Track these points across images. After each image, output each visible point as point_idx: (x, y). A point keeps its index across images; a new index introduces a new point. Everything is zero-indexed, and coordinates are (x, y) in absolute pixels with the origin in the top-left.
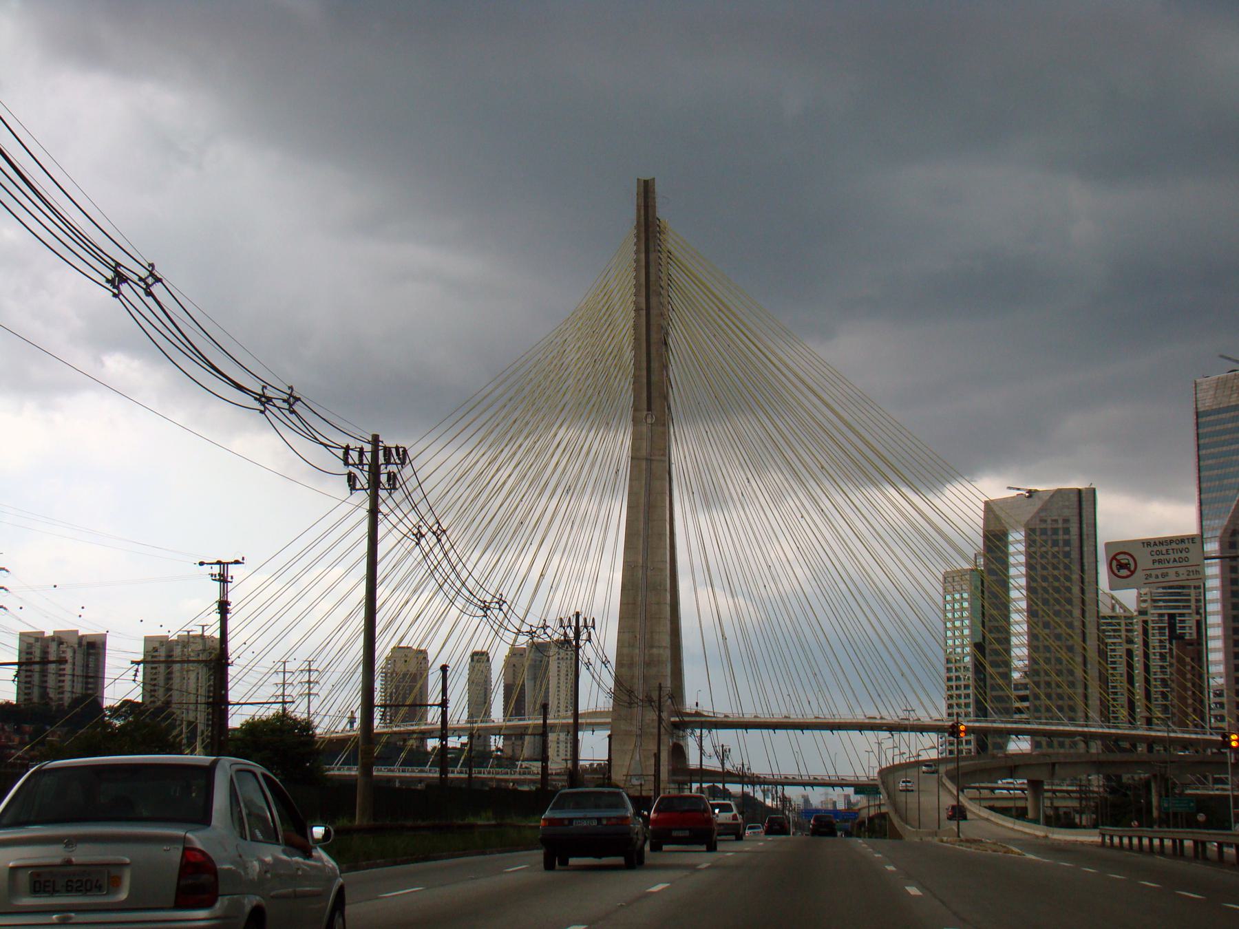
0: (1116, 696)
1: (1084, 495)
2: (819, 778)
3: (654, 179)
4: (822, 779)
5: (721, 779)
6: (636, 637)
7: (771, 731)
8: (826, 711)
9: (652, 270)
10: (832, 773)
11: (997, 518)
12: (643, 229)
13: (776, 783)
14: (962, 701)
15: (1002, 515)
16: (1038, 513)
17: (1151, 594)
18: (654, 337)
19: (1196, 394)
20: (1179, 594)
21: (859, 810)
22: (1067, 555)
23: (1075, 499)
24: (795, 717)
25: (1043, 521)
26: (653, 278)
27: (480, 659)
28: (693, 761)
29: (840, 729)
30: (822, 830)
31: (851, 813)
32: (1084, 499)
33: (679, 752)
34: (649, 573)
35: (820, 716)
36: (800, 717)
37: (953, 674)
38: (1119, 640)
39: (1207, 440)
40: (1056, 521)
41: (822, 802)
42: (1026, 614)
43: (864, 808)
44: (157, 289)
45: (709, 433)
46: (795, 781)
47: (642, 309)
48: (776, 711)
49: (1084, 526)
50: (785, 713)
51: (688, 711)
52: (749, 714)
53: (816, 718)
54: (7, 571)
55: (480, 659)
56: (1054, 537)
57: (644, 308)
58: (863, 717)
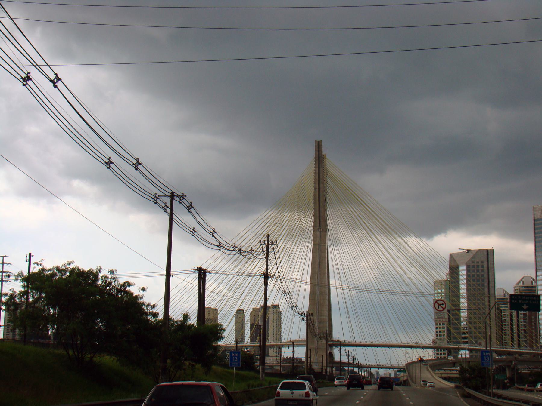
0: (506, 334)
1: (489, 252)
2: (384, 365)
3: (321, 141)
4: (385, 366)
5: (348, 366)
6: (315, 312)
7: (366, 348)
8: (387, 341)
9: (321, 175)
10: (389, 363)
11: (455, 261)
12: (317, 159)
13: (368, 367)
14: (442, 333)
15: (457, 259)
16: (471, 259)
17: (519, 289)
18: (321, 200)
19: (534, 212)
20: (531, 290)
21: (400, 377)
22: (483, 276)
23: (486, 253)
24: (375, 342)
25: (473, 262)
26: (321, 177)
27: (240, 312)
28: (337, 358)
29: (392, 347)
30: (385, 386)
31: (396, 379)
32: (489, 253)
33: (331, 355)
34: (320, 288)
35: (385, 342)
36: (377, 342)
37: (438, 330)
38: (507, 308)
39: (538, 231)
40: (478, 262)
41: (384, 374)
42: (466, 299)
43: (401, 377)
44: (215, 235)
45: (342, 234)
46: (375, 366)
47: (317, 189)
48: (367, 340)
49: (489, 264)
50: (371, 341)
51: (334, 340)
52: (358, 341)
53: (383, 343)
54: (11, 264)
55: (240, 312)
56: (478, 269)
57: (318, 188)
58: (401, 343)
